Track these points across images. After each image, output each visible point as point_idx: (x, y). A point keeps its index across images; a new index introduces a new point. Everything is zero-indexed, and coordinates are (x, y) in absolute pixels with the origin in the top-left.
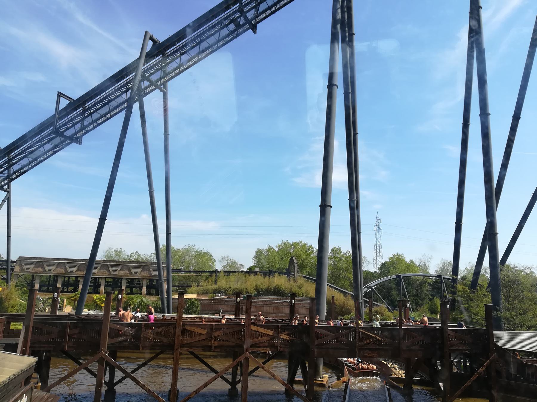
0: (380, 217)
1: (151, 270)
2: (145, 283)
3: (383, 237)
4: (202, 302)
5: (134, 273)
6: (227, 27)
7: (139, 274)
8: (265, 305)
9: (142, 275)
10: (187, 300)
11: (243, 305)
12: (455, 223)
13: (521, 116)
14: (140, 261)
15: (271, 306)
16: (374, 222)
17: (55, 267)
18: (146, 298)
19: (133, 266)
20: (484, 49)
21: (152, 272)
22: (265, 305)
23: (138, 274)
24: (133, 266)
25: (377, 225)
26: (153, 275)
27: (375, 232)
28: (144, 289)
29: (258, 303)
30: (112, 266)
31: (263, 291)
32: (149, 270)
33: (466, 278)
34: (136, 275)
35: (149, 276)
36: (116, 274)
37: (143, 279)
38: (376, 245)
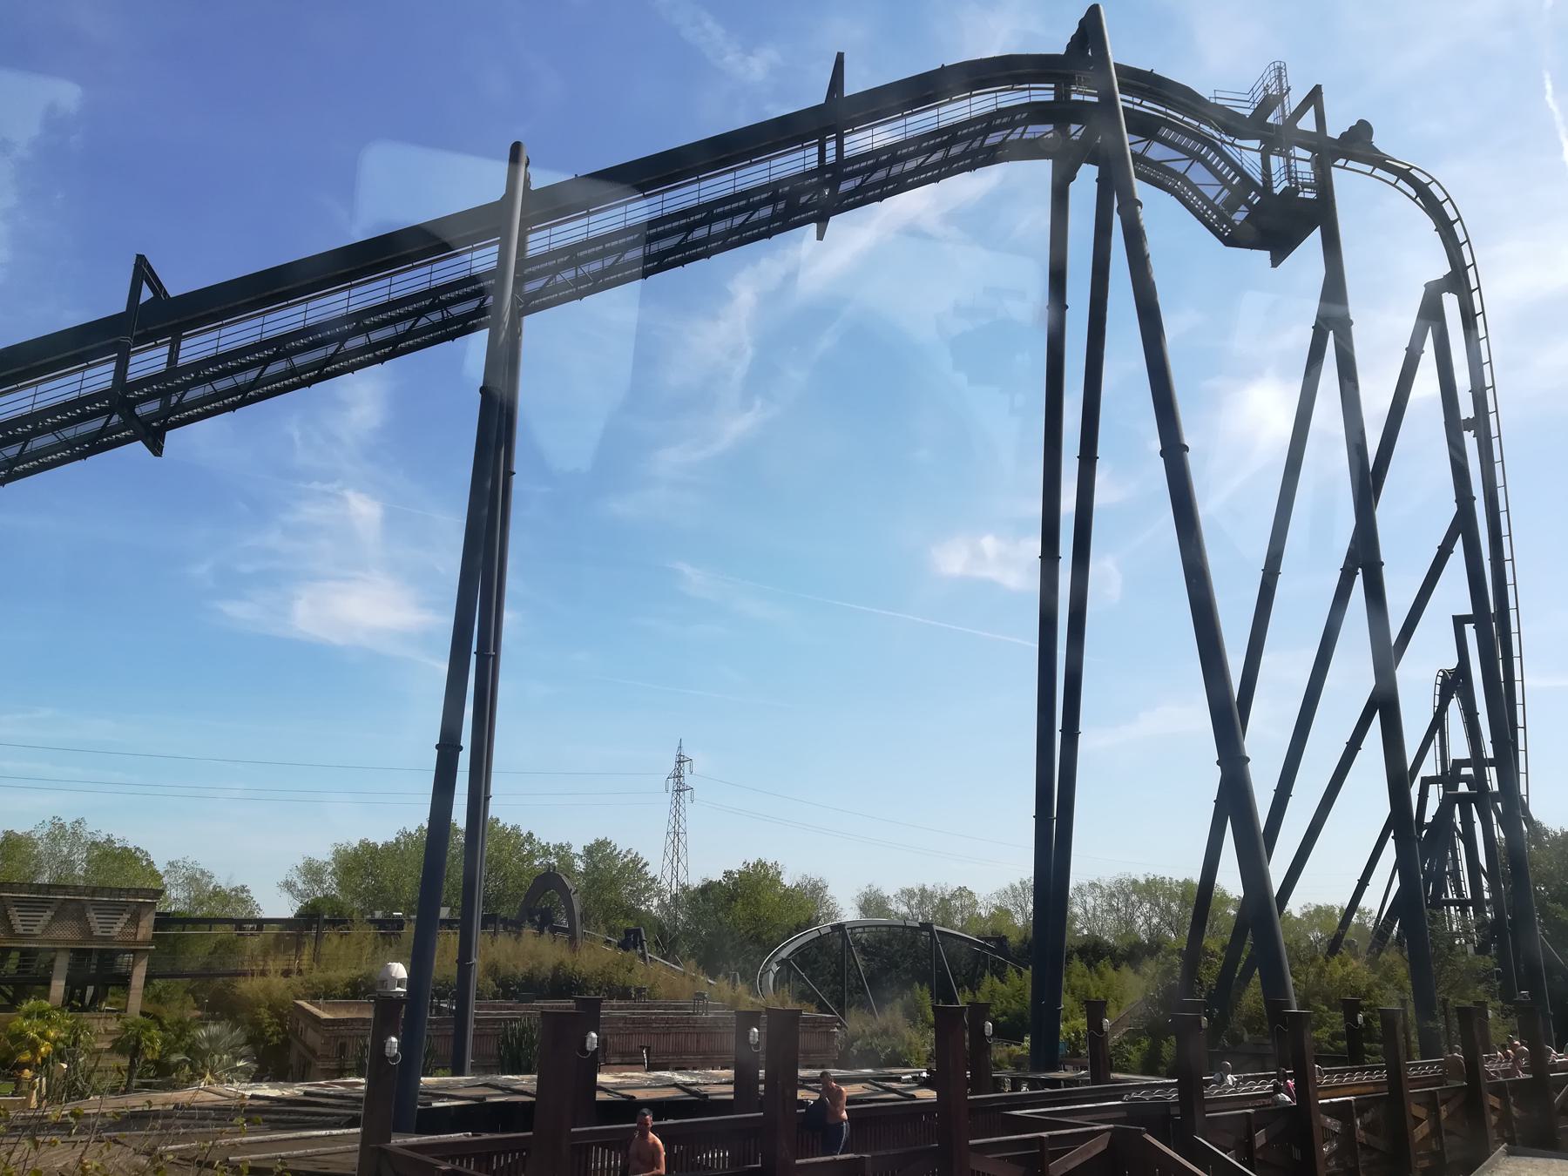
0: (686, 753)
1: (91, 915)
2: (62, 963)
3: (691, 810)
4: (437, 1029)
5: (20, 929)
6: (1053, 92)
7: (40, 932)
8: (673, 1030)
9: (54, 936)
10: (506, 1025)
11: (607, 1031)
12: (437, 746)
13: (133, 267)
14: (45, 879)
15: (691, 1030)
16: (671, 766)
17: (49, 918)
18: (102, 1021)
19: (20, 903)
20: (1149, 255)
21: (92, 924)
22: (673, 1030)
23: (36, 931)
24: (20, 903)
25: (678, 776)
26: (95, 934)
27: (668, 797)
28: (58, 987)
29: (654, 1025)
30: (100, 908)
31: (518, 985)
32: (81, 917)
33: (1159, 947)
34: (28, 936)
35: (78, 938)
36: (35, 935)
37: (55, 950)
38: (672, 836)
